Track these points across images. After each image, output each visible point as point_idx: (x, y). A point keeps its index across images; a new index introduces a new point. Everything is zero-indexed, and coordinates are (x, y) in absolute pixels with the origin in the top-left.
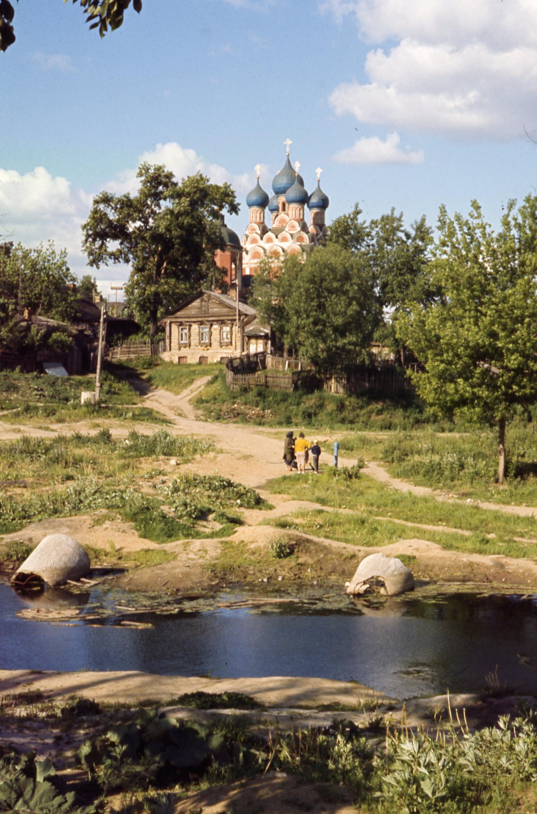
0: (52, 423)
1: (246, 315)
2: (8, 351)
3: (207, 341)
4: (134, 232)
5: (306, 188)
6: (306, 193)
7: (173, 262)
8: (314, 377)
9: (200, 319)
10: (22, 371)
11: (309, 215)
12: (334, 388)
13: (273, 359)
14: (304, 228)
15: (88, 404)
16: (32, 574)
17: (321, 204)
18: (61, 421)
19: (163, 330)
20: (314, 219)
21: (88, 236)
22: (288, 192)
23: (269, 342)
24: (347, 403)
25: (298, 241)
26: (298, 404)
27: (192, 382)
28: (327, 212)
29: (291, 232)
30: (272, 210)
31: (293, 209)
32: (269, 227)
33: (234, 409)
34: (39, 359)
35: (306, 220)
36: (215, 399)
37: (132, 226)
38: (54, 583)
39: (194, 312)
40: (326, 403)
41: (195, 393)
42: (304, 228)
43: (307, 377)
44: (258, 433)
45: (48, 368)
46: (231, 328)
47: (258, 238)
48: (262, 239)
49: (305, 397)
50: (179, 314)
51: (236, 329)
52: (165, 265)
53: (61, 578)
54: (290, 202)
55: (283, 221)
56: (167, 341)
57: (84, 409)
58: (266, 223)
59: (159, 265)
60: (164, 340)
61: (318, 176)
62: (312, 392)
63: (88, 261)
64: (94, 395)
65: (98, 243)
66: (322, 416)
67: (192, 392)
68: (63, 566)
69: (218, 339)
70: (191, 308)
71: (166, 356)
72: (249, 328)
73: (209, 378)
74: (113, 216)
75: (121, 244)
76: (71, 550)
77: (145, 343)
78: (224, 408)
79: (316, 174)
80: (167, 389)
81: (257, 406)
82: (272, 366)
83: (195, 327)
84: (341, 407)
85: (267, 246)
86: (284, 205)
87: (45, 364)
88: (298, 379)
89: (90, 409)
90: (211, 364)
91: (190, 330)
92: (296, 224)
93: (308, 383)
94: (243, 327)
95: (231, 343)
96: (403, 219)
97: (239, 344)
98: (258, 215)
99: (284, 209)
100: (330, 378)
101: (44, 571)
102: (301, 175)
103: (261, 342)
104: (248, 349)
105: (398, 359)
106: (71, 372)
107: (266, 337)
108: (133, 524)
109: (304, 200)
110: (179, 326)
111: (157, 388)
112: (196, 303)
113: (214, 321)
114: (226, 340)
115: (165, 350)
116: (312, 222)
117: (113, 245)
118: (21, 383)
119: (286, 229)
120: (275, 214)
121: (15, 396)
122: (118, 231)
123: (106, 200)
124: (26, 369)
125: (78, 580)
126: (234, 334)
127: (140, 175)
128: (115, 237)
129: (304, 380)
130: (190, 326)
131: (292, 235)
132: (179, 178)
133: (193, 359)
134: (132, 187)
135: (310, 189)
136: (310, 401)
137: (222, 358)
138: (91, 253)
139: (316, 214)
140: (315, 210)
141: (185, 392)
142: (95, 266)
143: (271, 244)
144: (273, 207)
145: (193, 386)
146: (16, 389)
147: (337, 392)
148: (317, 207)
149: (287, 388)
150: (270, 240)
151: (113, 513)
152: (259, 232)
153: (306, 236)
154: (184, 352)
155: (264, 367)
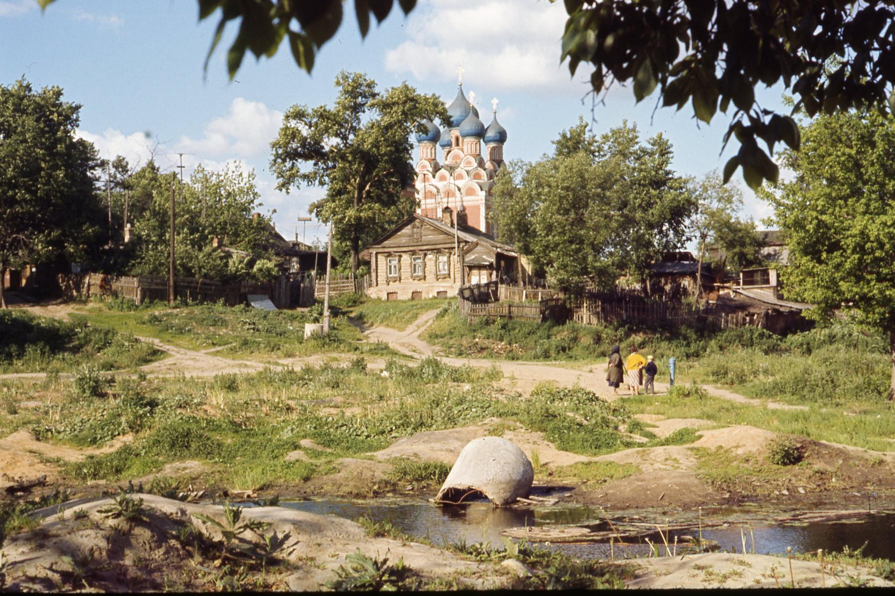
0: (279, 357)
1: (466, 242)
2: (208, 281)
3: (421, 274)
4: (332, 151)
5: (482, 118)
6: (483, 126)
7: (378, 184)
8: (563, 306)
9: (411, 248)
10: (224, 305)
11: (486, 151)
12: (586, 317)
13: (506, 289)
14: (481, 164)
15: (315, 336)
16: (470, 489)
17: (498, 138)
18: (289, 355)
19: (367, 263)
20: (491, 154)
21: (278, 156)
22: (461, 125)
23: (494, 273)
24: (604, 336)
25: (475, 178)
26: (549, 337)
27: (416, 317)
28: (505, 146)
29: (467, 169)
30: (443, 146)
31: (469, 143)
32: (441, 164)
33: (477, 343)
34: (243, 290)
35: (483, 155)
36: (451, 333)
37: (330, 143)
38: (502, 500)
39: (404, 240)
40: (581, 335)
41: (423, 329)
42: (481, 164)
43: (555, 306)
44: (555, 365)
45: (254, 301)
46: (449, 257)
47: (430, 176)
48: (434, 177)
49: (555, 328)
50: (386, 243)
51: (455, 258)
52: (367, 188)
53: (508, 494)
54: (464, 136)
55: (456, 157)
56: (373, 275)
57: (313, 342)
58: (438, 160)
59: (361, 187)
60: (369, 273)
61: (494, 107)
62: (564, 323)
63: (276, 185)
64: (322, 327)
65: (288, 164)
66: (577, 351)
67: (419, 327)
68: (508, 478)
69: (434, 271)
70: (400, 236)
71: (372, 293)
72: (470, 258)
73: (438, 311)
74: (305, 131)
75: (315, 164)
76: (513, 457)
77: (347, 278)
78: (464, 343)
79: (492, 105)
80: (387, 326)
81: (501, 340)
82: (506, 297)
83: (406, 258)
84: (598, 340)
85: (441, 185)
86: (457, 139)
87: (249, 296)
88: (546, 309)
89: (320, 342)
90: (425, 299)
91: (399, 261)
92: (473, 160)
93: (557, 314)
94: (463, 255)
95: (449, 275)
96: (637, 129)
97: (459, 276)
98: (429, 150)
99: (458, 145)
100: (580, 307)
101: (485, 485)
102: (476, 106)
103: (484, 273)
104: (469, 281)
105: (644, 289)
106: (279, 306)
107: (490, 267)
108: (542, 434)
109: (480, 133)
110: (388, 256)
111: (372, 325)
112: (407, 230)
113: (428, 250)
114: (443, 272)
115: (370, 285)
116: (489, 158)
117: (306, 166)
118: (229, 317)
119: (461, 166)
120: (447, 149)
121: (224, 330)
122: (313, 151)
123: (299, 115)
124: (231, 302)
125: (527, 498)
126: (452, 264)
127: (338, 83)
128: (306, 157)
129: (552, 309)
130: (400, 256)
131: (468, 172)
132: (383, 90)
133: (404, 295)
134: (331, 99)
135: (486, 119)
136: (562, 334)
137: (438, 293)
138: (281, 175)
139: (493, 149)
140: (492, 145)
141: (411, 328)
142: (284, 190)
143: (445, 183)
144: (445, 143)
145: (419, 321)
146: (224, 323)
147: (590, 323)
148: (494, 141)
149: (534, 319)
150: (443, 178)
151: (510, 421)
152: (431, 169)
153: (483, 173)
154: (393, 287)
155: (497, 299)
